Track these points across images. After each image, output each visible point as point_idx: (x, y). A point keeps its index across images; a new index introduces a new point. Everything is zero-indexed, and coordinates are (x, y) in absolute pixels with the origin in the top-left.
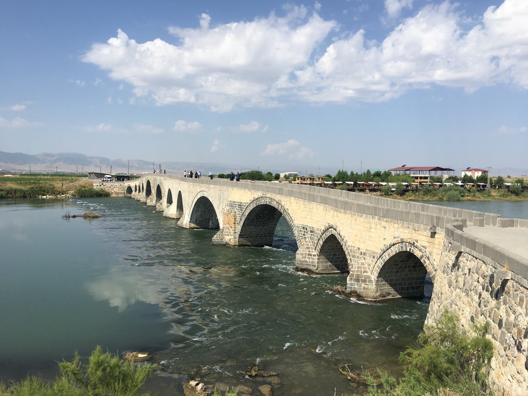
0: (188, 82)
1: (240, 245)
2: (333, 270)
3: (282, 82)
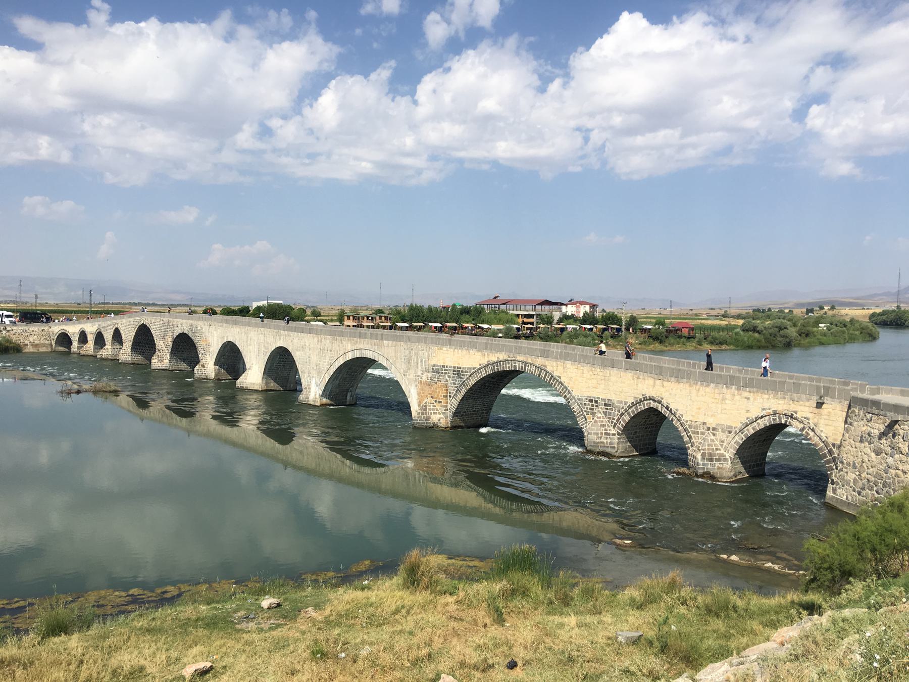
0: (53, 124)
1: (454, 427)
2: (632, 451)
3: (245, 137)
